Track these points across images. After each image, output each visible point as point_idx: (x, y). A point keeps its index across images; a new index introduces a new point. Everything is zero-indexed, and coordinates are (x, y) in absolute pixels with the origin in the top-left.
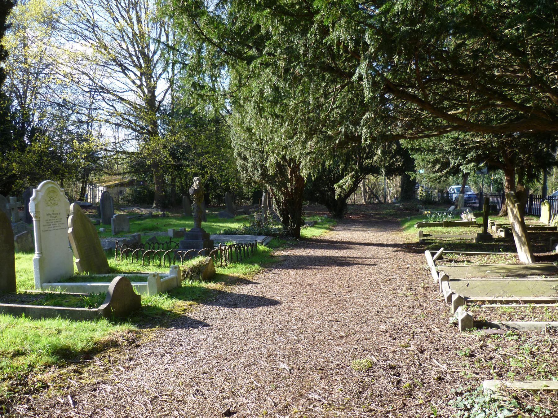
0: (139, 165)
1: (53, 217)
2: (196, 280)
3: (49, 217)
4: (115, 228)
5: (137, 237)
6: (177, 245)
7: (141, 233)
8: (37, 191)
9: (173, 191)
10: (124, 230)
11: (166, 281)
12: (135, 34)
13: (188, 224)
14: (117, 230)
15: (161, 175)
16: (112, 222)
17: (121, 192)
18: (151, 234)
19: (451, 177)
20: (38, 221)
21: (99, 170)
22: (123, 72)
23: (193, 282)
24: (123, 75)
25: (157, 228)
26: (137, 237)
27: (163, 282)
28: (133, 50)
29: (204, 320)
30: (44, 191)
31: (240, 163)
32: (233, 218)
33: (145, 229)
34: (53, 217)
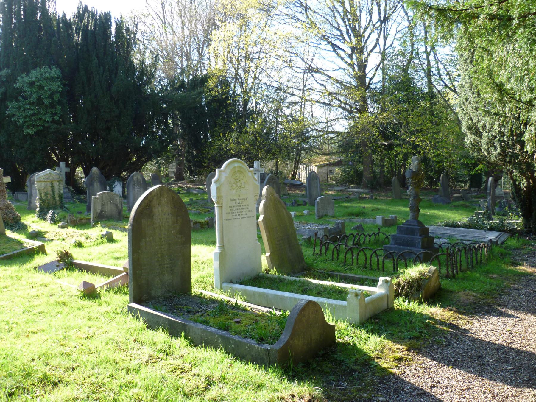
0: (348, 145)
1: (239, 203)
2: (414, 299)
3: (233, 204)
4: (318, 211)
5: (340, 225)
6: (387, 237)
7: (346, 219)
8: (220, 172)
9: (382, 172)
10: (329, 214)
11: (373, 301)
12: (345, 11)
13: (402, 211)
14: (320, 214)
15: (369, 155)
16: (316, 205)
17: (331, 172)
18: (357, 221)
19: (155, 168)
20: (221, 207)
21: (310, 150)
22: (335, 51)
23: (409, 302)
24: (334, 54)
25: (364, 213)
26: (340, 225)
27: (369, 303)
28: (343, 24)
29: (432, 387)
30: (228, 171)
31: (470, 138)
32: (449, 203)
33: (352, 214)
34: (239, 203)
